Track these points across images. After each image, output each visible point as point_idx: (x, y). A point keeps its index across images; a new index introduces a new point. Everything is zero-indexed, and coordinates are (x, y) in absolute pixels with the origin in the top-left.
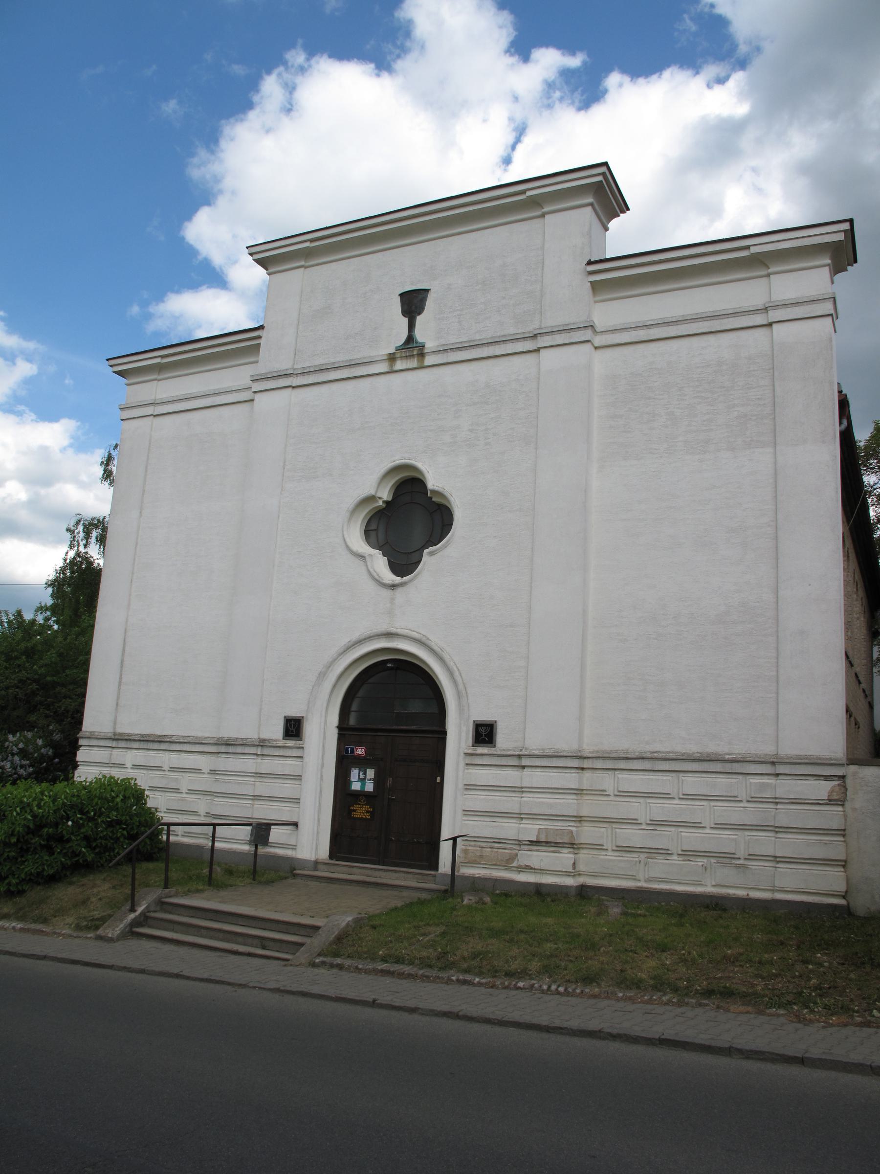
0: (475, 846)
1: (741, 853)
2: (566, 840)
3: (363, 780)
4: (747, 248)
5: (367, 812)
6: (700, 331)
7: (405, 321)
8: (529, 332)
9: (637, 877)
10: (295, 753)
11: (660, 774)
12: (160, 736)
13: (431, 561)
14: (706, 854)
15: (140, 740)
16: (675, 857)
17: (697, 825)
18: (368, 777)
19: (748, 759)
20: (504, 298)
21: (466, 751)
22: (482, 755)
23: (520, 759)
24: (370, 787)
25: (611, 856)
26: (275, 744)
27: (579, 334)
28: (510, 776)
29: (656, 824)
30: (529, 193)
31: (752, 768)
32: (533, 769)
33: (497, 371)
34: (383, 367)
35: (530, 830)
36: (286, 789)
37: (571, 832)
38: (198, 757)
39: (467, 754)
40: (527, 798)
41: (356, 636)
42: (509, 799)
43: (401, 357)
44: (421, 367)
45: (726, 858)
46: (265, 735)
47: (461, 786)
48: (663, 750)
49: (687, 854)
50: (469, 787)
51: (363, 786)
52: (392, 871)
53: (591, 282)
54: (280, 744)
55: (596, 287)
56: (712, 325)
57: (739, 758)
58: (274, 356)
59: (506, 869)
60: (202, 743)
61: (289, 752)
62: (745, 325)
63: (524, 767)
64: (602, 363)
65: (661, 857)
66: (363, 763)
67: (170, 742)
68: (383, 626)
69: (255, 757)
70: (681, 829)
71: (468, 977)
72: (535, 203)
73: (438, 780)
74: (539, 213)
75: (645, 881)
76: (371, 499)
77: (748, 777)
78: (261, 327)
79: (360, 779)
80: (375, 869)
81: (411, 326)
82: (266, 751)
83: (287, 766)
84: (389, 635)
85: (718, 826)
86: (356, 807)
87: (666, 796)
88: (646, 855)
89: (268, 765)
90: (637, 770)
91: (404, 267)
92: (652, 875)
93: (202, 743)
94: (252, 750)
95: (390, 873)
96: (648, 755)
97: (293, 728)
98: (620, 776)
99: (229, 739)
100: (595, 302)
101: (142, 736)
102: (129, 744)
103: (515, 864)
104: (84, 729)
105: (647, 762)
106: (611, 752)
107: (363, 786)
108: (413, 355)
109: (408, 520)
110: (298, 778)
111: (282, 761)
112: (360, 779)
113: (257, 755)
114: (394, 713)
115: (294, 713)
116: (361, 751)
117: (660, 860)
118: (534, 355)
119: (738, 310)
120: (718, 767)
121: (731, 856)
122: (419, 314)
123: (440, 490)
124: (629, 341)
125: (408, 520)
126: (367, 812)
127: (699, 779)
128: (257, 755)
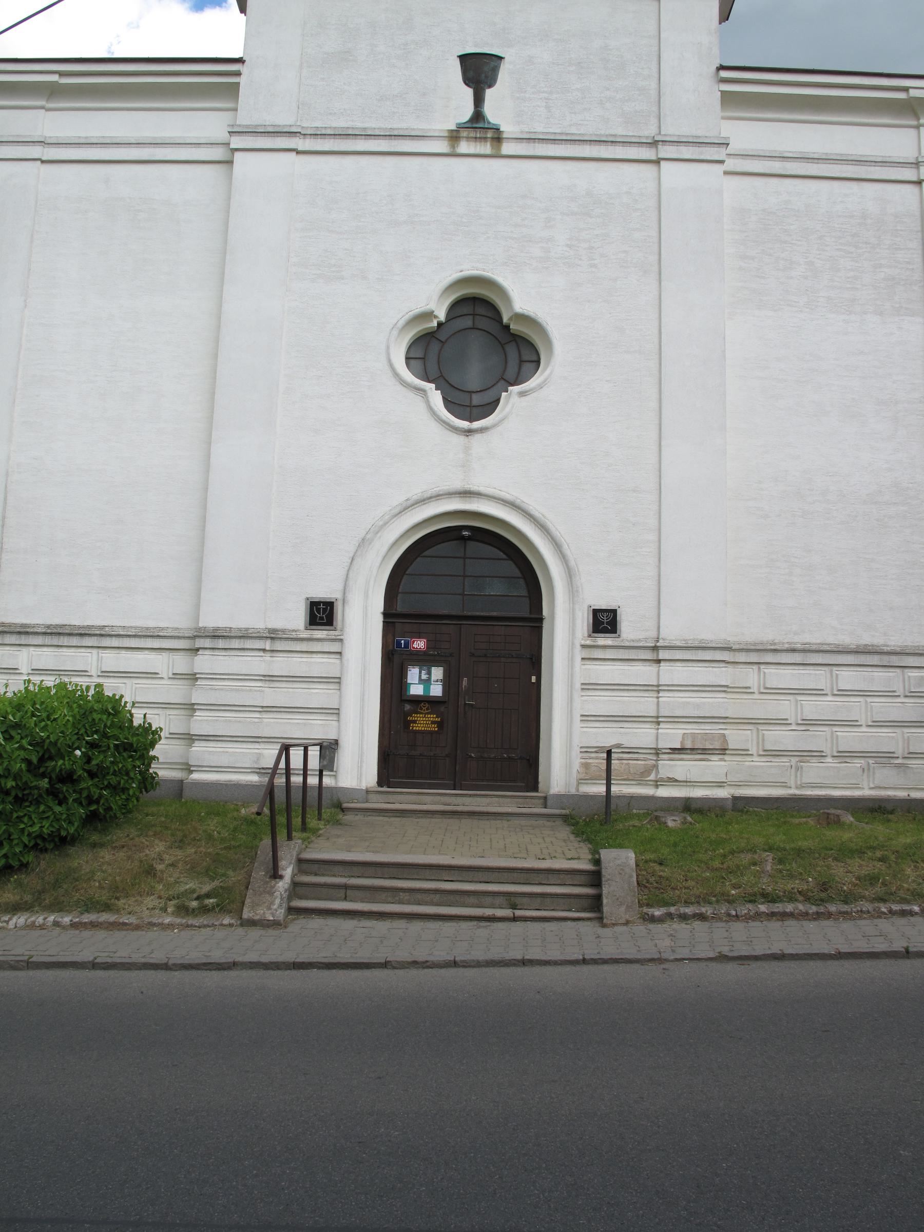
0: (597, 758)
2: (717, 745)
3: (427, 682)
4: (906, 89)
5: (433, 722)
6: (844, 175)
7: (469, 92)
8: (647, 137)
9: (788, 785)
10: (327, 647)
11: (812, 668)
12: (80, 627)
13: (513, 402)
14: (863, 755)
15: (45, 634)
16: (829, 760)
17: (852, 724)
18: (433, 678)
19: (907, 651)
20: (608, 89)
21: (583, 642)
22: (605, 647)
23: (655, 652)
24: (437, 690)
25: (759, 762)
26: (294, 635)
27: (705, 150)
28: (643, 673)
29: (808, 723)
32: (672, 664)
33: (604, 178)
34: (442, 146)
35: (672, 736)
36: (319, 696)
37: (724, 735)
38: (152, 656)
39: (583, 646)
41: (416, 492)
42: (642, 699)
43: (468, 138)
44: (497, 156)
45: (885, 758)
47: (578, 686)
48: (814, 641)
49: (844, 756)
51: (427, 689)
52: (470, 795)
53: (723, 93)
55: (728, 99)
57: (898, 649)
59: (639, 784)
60: (159, 636)
61: (317, 647)
62: (893, 178)
64: (736, 190)
65: (814, 760)
66: (425, 660)
67: (102, 635)
69: (261, 654)
70: (835, 729)
71: (906, 907)
73: (534, 679)
75: (797, 788)
76: (429, 315)
77: (906, 670)
78: (240, 61)
79: (421, 681)
80: (456, 795)
81: (479, 100)
82: (279, 645)
84: (466, 494)
86: (415, 717)
87: (818, 692)
88: (797, 759)
89: (281, 665)
90: (784, 664)
92: (805, 780)
93: (159, 636)
94: (258, 644)
95: (479, 799)
96: (799, 646)
97: (322, 614)
98: (766, 671)
99: (216, 629)
100: (723, 118)
101: (48, 627)
102: (23, 640)
103: (652, 777)
105: (796, 654)
106: (755, 644)
107: (427, 689)
108: (485, 138)
109: (476, 348)
110: (338, 681)
111: (305, 659)
112: (421, 681)
113: (264, 650)
114: (468, 603)
115: (321, 593)
116: (420, 644)
117: (814, 763)
119: (888, 160)
120: (875, 660)
122: (490, 86)
123: (532, 314)
124: (762, 171)
125: (476, 348)
126: (433, 722)
127: (854, 673)
128: (264, 650)
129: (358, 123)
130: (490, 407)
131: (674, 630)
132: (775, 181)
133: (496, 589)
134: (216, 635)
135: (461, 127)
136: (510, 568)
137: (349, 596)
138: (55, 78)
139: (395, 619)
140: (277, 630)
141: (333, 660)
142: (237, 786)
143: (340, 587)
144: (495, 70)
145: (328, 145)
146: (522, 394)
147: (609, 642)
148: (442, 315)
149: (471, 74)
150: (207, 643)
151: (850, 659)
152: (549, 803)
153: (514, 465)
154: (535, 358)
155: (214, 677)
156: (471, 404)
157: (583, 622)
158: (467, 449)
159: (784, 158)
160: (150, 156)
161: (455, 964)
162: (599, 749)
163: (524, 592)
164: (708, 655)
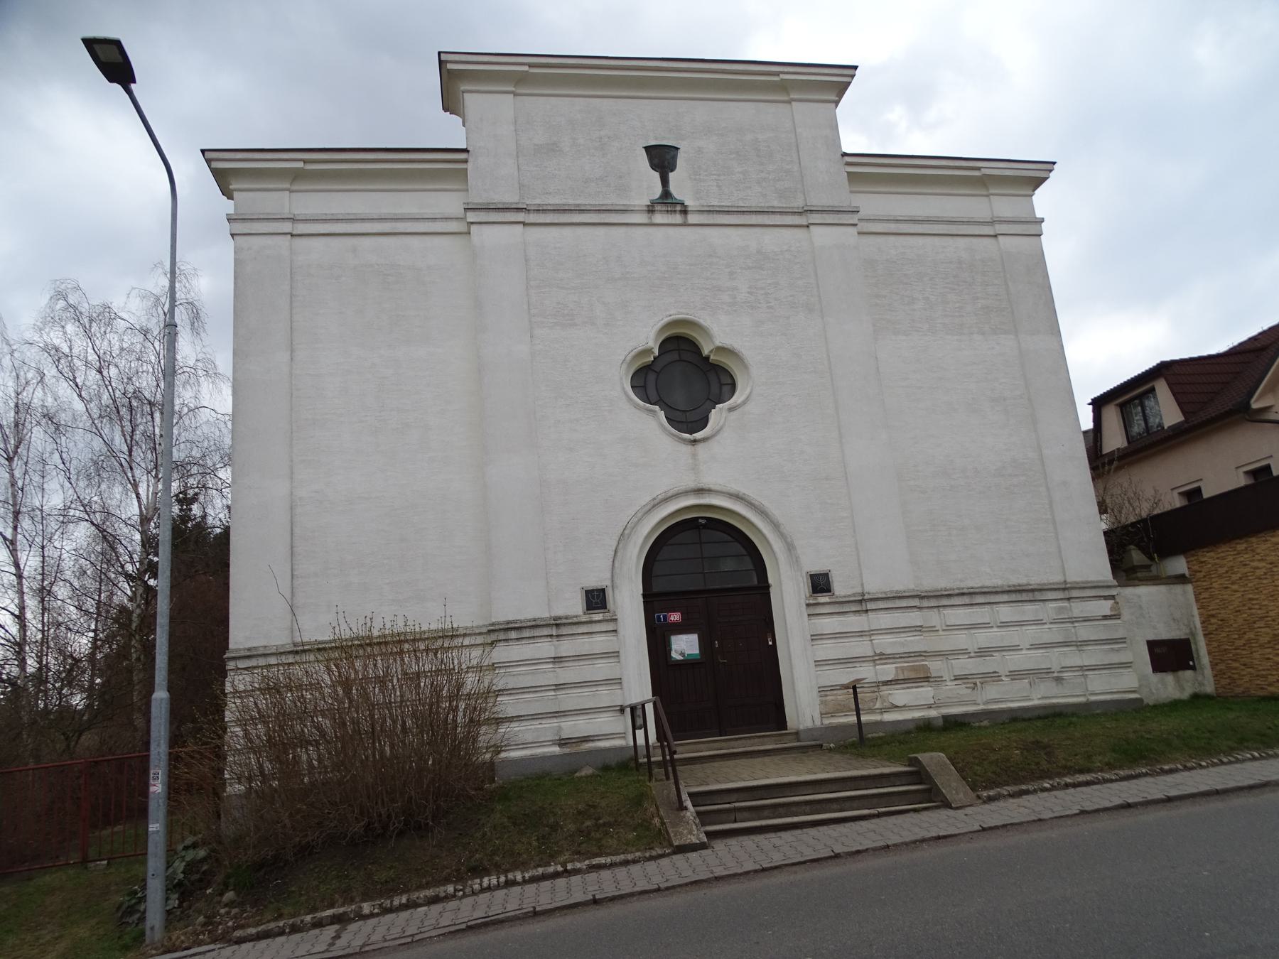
1: (1055, 668)
4: (979, 169)
10: (604, 627)
13: (717, 415)
17: (1015, 648)
23: (862, 603)
26: (575, 620)
27: (839, 215)
28: (855, 622)
30: (782, 76)
31: (1050, 595)
33: (772, 240)
35: (888, 671)
36: (602, 669)
39: (808, 605)
40: (878, 640)
44: (685, 224)
46: (559, 611)
50: (815, 637)
54: (584, 619)
56: (952, 228)
58: (482, 187)
63: (867, 611)
66: (681, 629)
68: (689, 482)
72: (784, 87)
74: (786, 98)
78: (466, 151)
81: (665, 181)
82: (564, 631)
83: (599, 643)
84: (700, 491)
85: (1034, 647)
87: (986, 626)
89: (567, 647)
91: (652, 119)
94: (546, 632)
100: (852, 192)
104: (231, 646)
111: (586, 639)
114: (707, 580)
115: (593, 583)
118: (804, 230)
121: (1048, 671)
128: (551, 636)
129: (572, 201)
130: (703, 423)
131: (874, 585)
132: (892, 238)
133: (728, 565)
134: (509, 627)
135: (653, 203)
136: (738, 548)
137: (617, 581)
138: (301, 165)
139: (653, 600)
140: (560, 618)
141: (610, 637)
142: (544, 758)
143: (609, 575)
144: (675, 158)
145: (778, 220)
146: (731, 409)
147: (1147, 574)
148: (656, 353)
149: (656, 161)
150: (502, 636)
151: (1005, 598)
152: (802, 736)
153: (730, 464)
154: (729, 381)
155: (508, 665)
156: (688, 420)
157: (805, 588)
158: (694, 456)
159: (434, 219)
160: (393, 228)
161: (535, 914)
162: (845, 687)
163: (751, 567)
164: (904, 603)
